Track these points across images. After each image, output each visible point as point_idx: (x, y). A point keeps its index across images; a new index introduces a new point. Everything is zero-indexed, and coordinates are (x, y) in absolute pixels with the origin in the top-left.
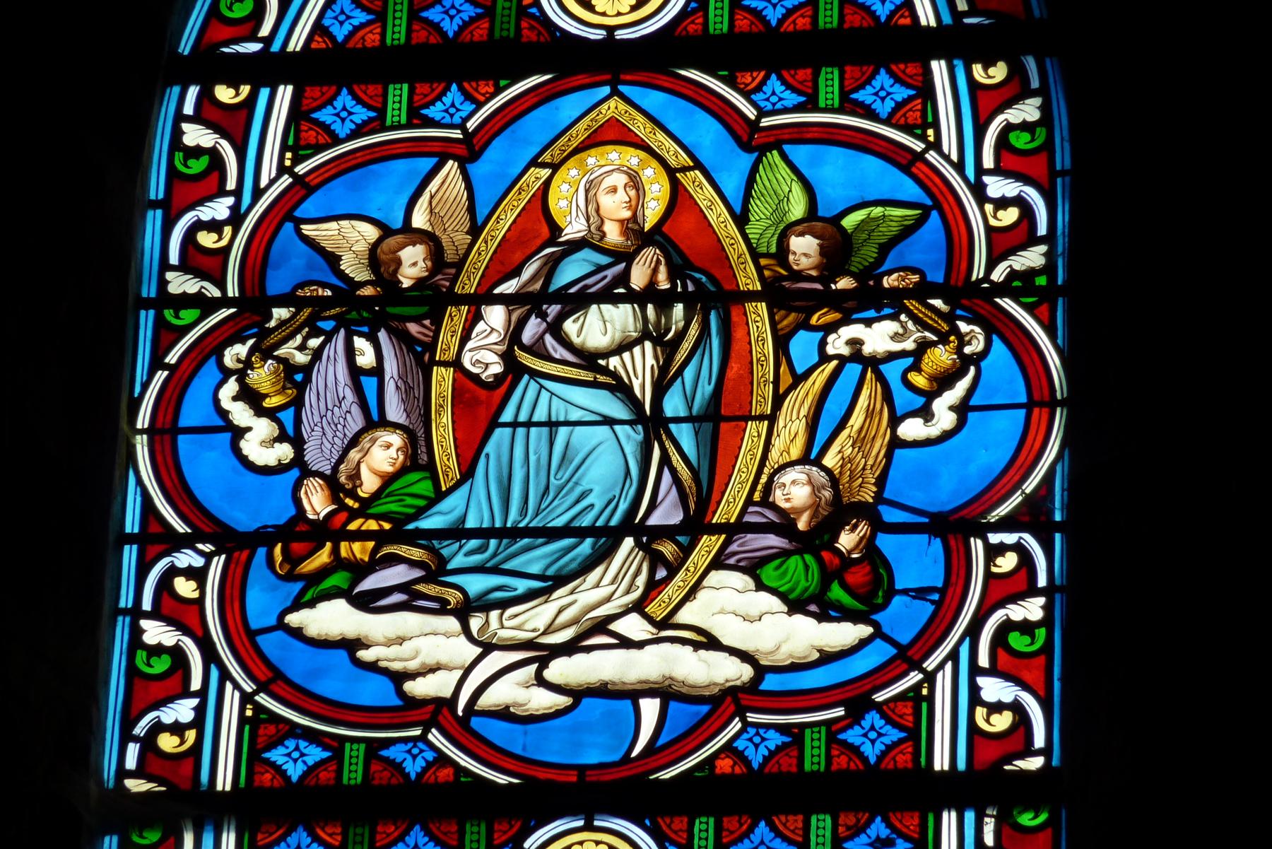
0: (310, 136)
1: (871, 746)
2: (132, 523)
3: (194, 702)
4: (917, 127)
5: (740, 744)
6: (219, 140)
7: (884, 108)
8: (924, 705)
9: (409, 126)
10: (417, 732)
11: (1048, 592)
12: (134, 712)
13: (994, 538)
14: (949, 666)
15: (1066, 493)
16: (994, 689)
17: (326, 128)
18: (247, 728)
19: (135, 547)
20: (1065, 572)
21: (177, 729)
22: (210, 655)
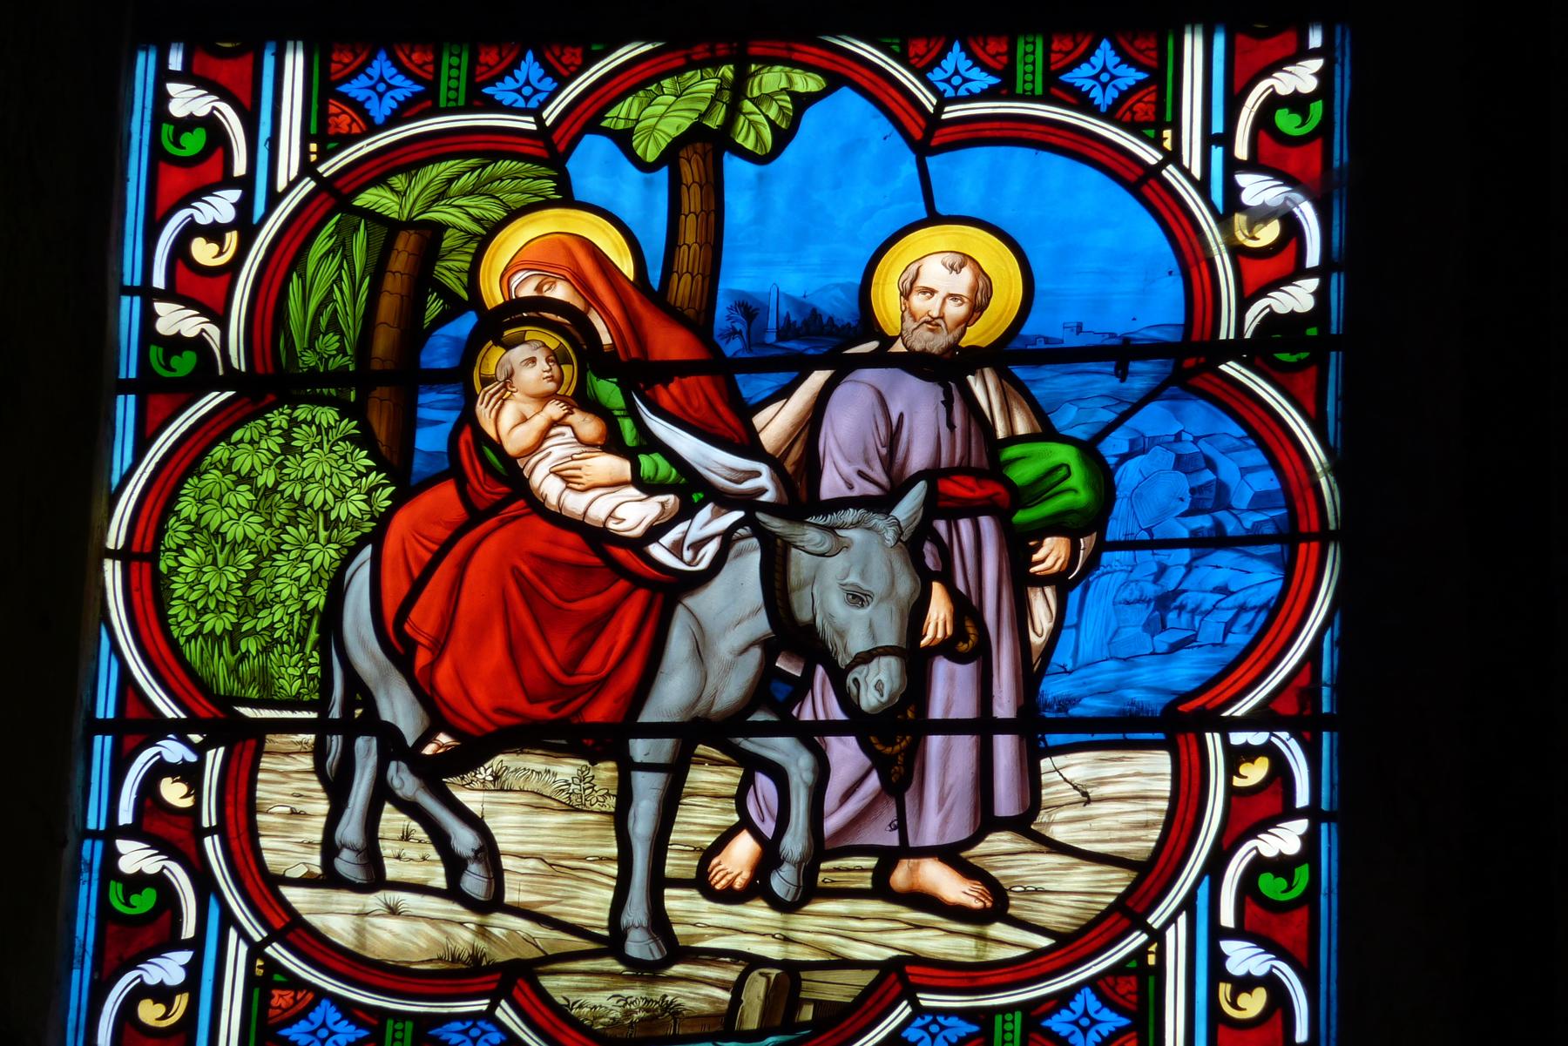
1: (1107, 64)
2: (106, 708)
3: (185, 956)
4: (1149, 125)
5: (548, 84)
6: (205, 326)
7: (1104, 99)
9: (468, 108)
10: (481, 1005)
12: (159, 213)
13: (1237, 738)
14: (1182, 920)
15: (1339, 403)
16: (1243, 958)
17: (358, 107)
18: (256, 993)
19: (132, 398)
20: (1342, 294)
21: (162, 994)
22: (205, 885)
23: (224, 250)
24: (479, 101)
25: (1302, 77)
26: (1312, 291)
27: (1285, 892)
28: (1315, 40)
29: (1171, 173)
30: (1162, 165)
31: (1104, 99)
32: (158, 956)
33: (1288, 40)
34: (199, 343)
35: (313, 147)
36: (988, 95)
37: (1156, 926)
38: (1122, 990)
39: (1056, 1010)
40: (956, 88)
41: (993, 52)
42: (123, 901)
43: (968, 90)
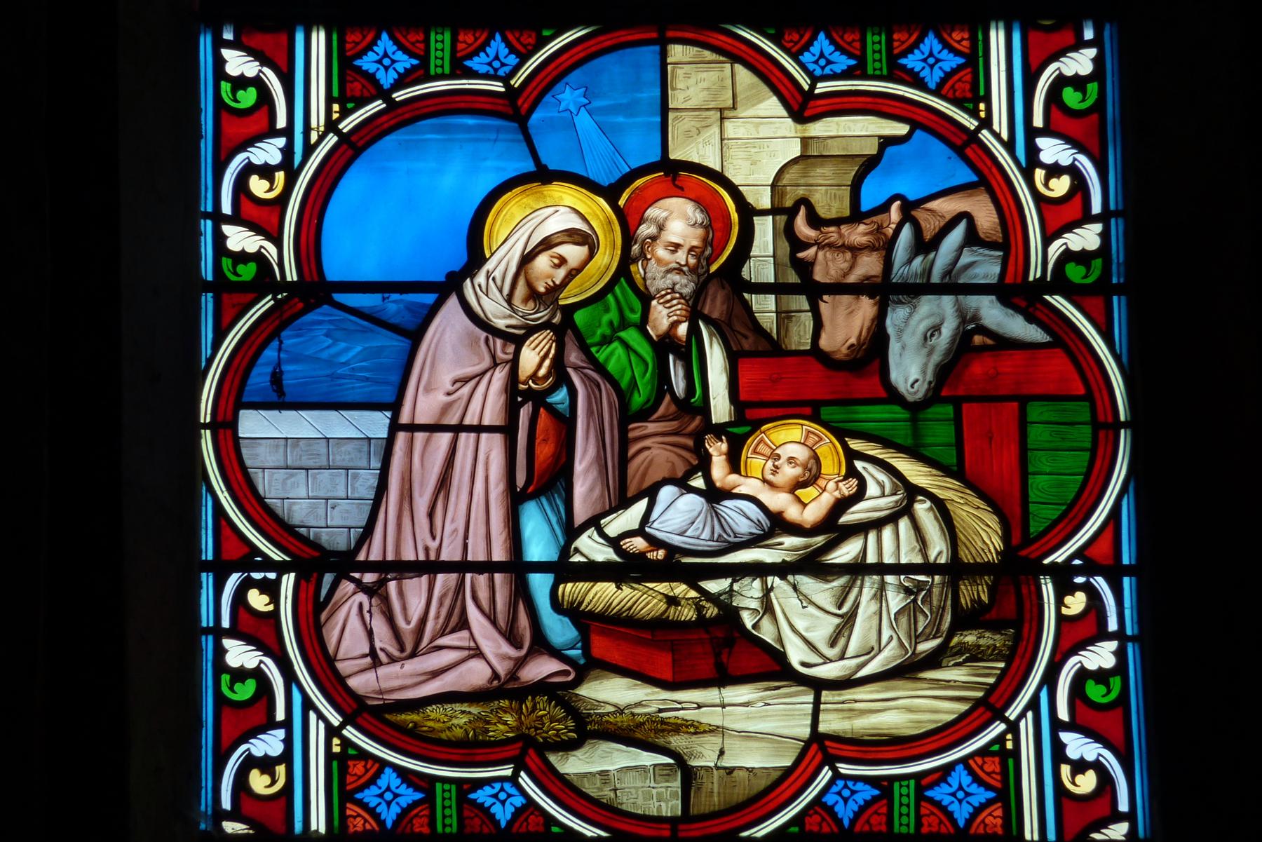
0: (356, 87)
3: (281, 142)
4: (353, 757)
5: (830, 799)
7: (933, 78)
8: (1011, 762)
9: (452, 76)
10: (507, 771)
11: (1104, 217)
14: (1030, 714)
16: (1078, 746)
21: (266, 765)
23: (274, 188)
24: (458, 70)
25: (1080, 63)
26: (1098, 233)
27: (1103, 696)
28: (1089, 34)
29: (985, 135)
30: (978, 129)
31: (389, 778)
32: (264, 732)
33: (1069, 37)
34: (259, 257)
35: (336, 107)
36: (847, 74)
37: (1012, 718)
38: (988, 768)
39: (936, 783)
40: (502, 789)
41: (849, 40)
42: (1043, 182)
43: (493, 788)
